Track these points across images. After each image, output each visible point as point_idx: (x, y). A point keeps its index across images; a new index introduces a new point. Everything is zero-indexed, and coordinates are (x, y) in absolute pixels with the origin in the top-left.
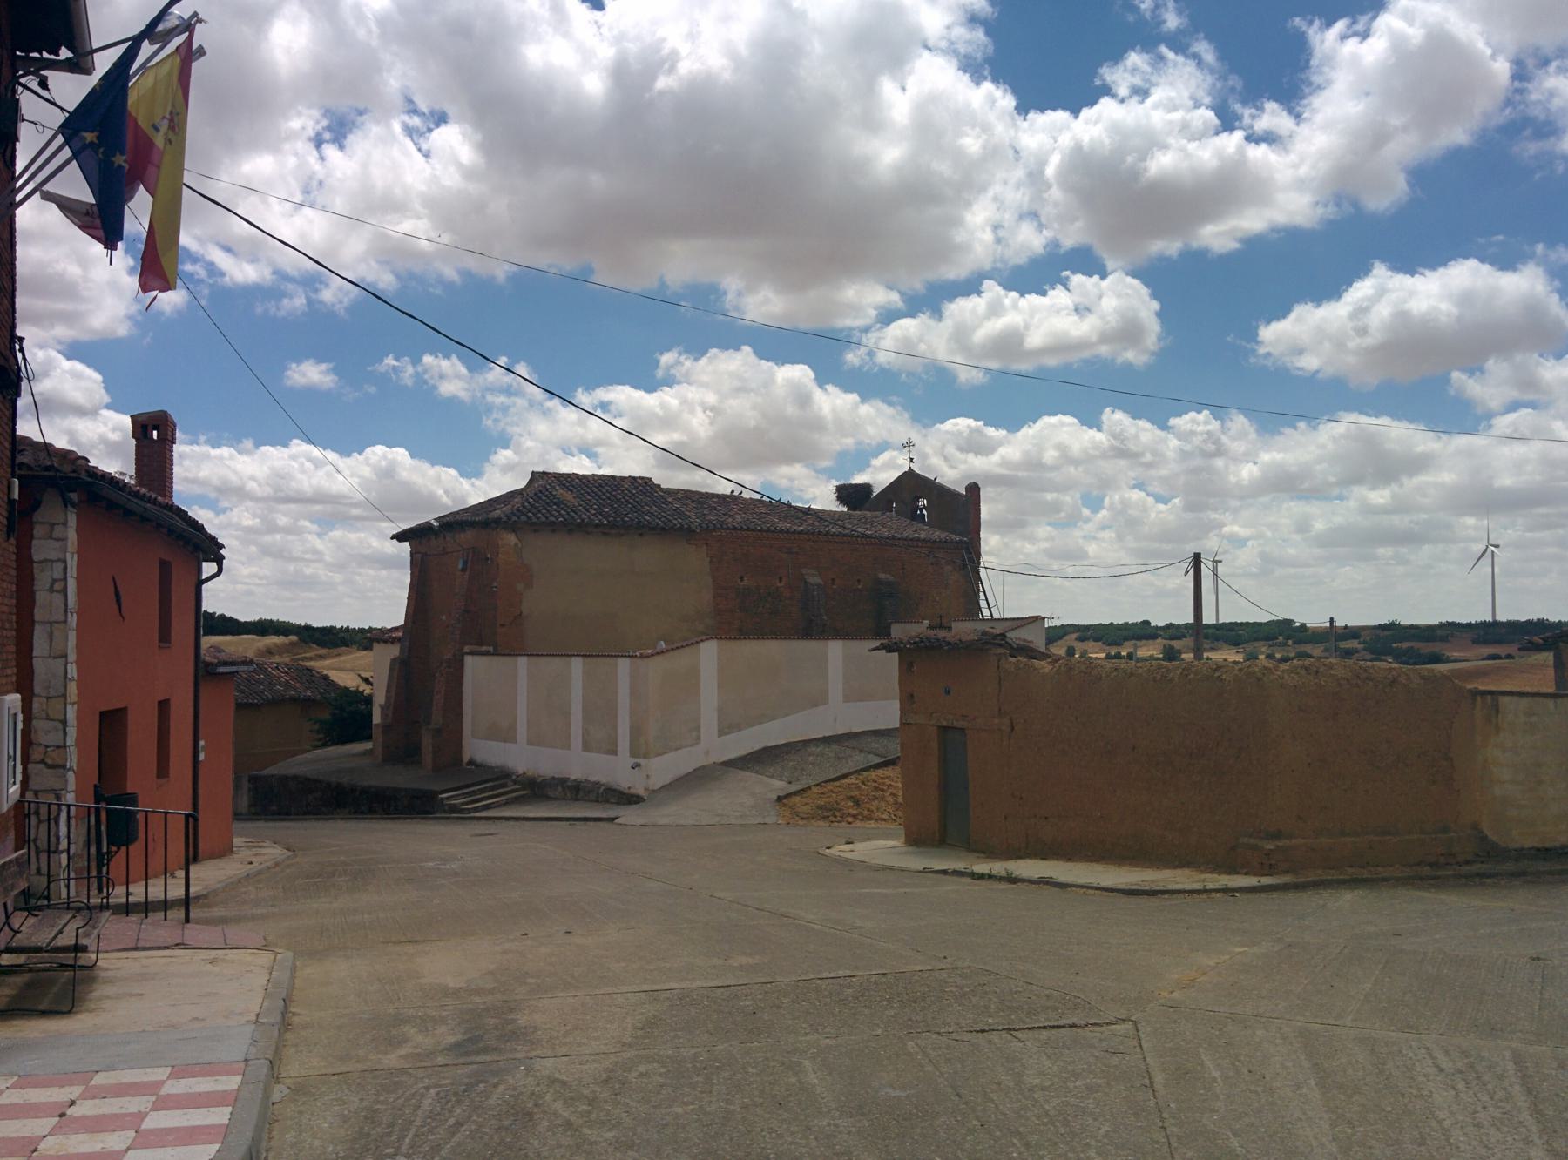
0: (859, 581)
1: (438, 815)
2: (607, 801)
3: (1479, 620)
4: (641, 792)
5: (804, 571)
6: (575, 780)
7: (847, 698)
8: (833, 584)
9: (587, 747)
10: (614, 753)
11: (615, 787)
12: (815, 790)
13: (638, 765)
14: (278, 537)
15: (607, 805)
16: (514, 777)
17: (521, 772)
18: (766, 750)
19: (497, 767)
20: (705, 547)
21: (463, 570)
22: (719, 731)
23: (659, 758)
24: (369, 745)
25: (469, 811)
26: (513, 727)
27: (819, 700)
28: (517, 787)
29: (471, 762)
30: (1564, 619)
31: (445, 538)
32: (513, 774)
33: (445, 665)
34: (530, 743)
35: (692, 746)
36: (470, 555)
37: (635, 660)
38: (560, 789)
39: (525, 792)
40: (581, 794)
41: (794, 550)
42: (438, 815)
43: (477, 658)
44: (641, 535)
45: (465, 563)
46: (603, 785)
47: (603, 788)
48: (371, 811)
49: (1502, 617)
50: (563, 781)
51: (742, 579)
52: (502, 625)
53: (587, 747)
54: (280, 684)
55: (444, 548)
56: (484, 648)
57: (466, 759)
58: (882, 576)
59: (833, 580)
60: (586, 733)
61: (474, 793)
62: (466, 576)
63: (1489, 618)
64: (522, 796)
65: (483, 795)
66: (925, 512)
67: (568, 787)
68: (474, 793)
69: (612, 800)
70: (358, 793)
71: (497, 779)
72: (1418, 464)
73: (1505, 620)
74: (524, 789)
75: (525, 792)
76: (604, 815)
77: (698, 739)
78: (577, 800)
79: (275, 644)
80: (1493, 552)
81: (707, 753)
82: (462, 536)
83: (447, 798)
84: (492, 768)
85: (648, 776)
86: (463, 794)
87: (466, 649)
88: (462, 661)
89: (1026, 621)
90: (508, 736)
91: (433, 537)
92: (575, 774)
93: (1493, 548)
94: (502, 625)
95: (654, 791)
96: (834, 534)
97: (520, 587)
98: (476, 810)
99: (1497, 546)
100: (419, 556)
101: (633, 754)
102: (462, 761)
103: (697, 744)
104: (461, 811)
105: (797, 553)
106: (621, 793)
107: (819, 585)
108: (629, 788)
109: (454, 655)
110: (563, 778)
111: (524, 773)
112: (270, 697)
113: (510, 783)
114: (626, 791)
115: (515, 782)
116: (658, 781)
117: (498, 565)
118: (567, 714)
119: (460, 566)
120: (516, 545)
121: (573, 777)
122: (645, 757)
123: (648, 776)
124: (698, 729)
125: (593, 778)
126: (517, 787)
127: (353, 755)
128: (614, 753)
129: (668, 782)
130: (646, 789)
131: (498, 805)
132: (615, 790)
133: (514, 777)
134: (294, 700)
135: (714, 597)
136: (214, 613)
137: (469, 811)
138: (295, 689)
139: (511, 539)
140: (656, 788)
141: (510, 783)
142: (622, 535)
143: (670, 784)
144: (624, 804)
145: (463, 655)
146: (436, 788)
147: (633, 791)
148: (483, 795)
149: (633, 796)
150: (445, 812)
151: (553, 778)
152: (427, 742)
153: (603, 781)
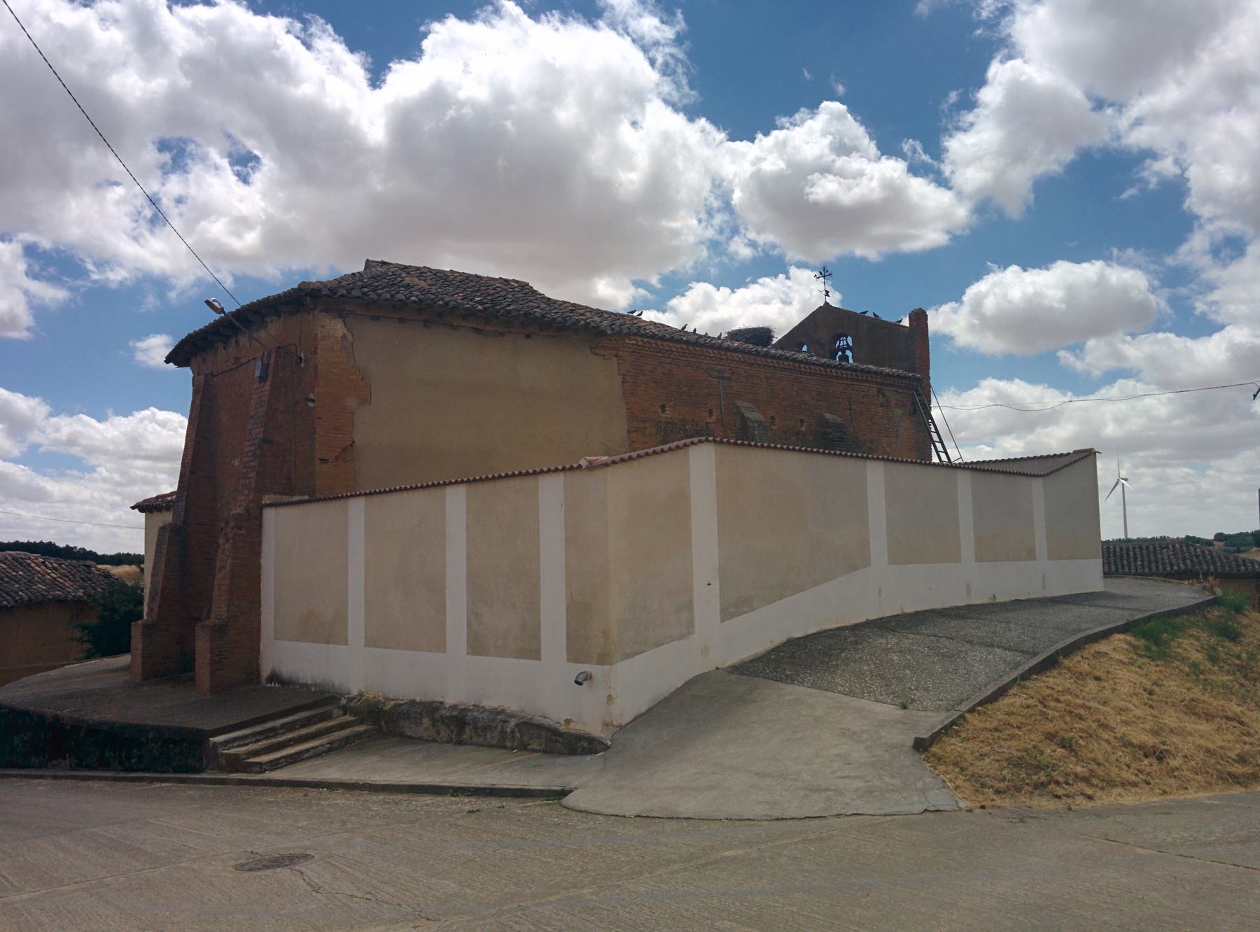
0: (802, 421)
1: (205, 776)
2: (524, 747)
3: (1115, 538)
4: (596, 730)
5: (739, 403)
6: (454, 707)
7: (894, 559)
8: (773, 423)
9: (477, 646)
10: (535, 654)
11: (539, 720)
12: (974, 720)
13: (589, 677)
14: (136, 488)
15: (526, 756)
16: (343, 701)
17: (355, 693)
18: (793, 645)
19: (315, 685)
20: (615, 359)
21: (263, 379)
22: (722, 611)
23: (630, 660)
24: (125, 659)
25: (262, 768)
26: (342, 616)
27: (856, 560)
28: (348, 718)
29: (274, 677)
30: (1258, 529)
31: (237, 342)
32: (342, 695)
33: (232, 524)
34: (370, 642)
35: (681, 637)
36: (273, 356)
37: (576, 475)
38: (426, 721)
39: (361, 728)
40: (468, 731)
41: (727, 375)
42: (205, 776)
43: (283, 511)
44: (528, 336)
45: (265, 368)
46: (512, 716)
47: (513, 722)
48: (103, 764)
49: (1133, 536)
50: (431, 709)
51: (663, 408)
52: (323, 461)
53: (477, 646)
54: (44, 582)
55: (237, 359)
56: (296, 498)
57: (266, 672)
58: (828, 416)
59: (773, 418)
60: (474, 618)
61: (274, 732)
62: (267, 387)
63: (1123, 537)
64: (358, 736)
65: (290, 736)
66: (848, 353)
67: (442, 719)
68: (274, 732)
69: (534, 746)
70: (82, 734)
71: (315, 705)
72: (1051, 417)
73: (1135, 538)
74: (361, 722)
75: (361, 728)
76: (535, 781)
77: (689, 629)
78: (460, 743)
79: (128, 573)
80: (1123, 484)
81: (705, 651)
82: (262, 333)
83: (226, 743)
84: (305, 686)
85: (610, 697)
86: (254, 734)
87: (267, 499)
88: (259, 518)
89: (1069, 460)
90: (332, 633)
91: (221, 346)
92: (454, 694)
93: (1123, 481)
94: (323, 461)
95: (621, 727)
96: (773, 357)
97: (351, 402)
98: (274, 765)
99: (1126, 480)
100: (202, 377)
101: (575, 654)
102: (259, 675)
103: (689, 633)
104: (247, 768)
105: (730, 379)
106: (555, 732)
107: (760, 423)
108: (568, 721)
109: (247, 510)
110: (432, 703)
111: (361, 695)
112: (26, 598)
113: (336, 712)
114: (563, 728)
115: (345, 710)
116: (629, 705)
117: (315, 366)
118: (437, 588)
119: (257, 374)
120: (344, 336)
121: (449, 701)
122: (604, 659)
123: (610, 697)
124: (689, 606)
125: (491, 703)
126: (348, 718)
127: (112, 671)
128: (535, 654)
129: (644, 709)
130: (606, 725)
131: (316, 754)
132: (540, 727)
133: (343, 701)
134: (61, 602)
135: (629, 432)
136: (76, 547)
137: (262, 768)
138: (63, 588)
139: (336, 328)
140: (623, 724)
141: (336, 712)
142: (502, 334)
143: (649, 710)
144: (561, 754)
145: (261, 508)
146: (205, 724)
147: (576, 727)
148: (290, 736)
149: (579, 738)
150: (221, 769)
151: (413, 703)
152: (202, 645)
153: (512, 706)
